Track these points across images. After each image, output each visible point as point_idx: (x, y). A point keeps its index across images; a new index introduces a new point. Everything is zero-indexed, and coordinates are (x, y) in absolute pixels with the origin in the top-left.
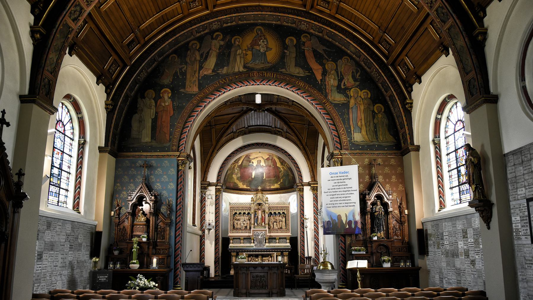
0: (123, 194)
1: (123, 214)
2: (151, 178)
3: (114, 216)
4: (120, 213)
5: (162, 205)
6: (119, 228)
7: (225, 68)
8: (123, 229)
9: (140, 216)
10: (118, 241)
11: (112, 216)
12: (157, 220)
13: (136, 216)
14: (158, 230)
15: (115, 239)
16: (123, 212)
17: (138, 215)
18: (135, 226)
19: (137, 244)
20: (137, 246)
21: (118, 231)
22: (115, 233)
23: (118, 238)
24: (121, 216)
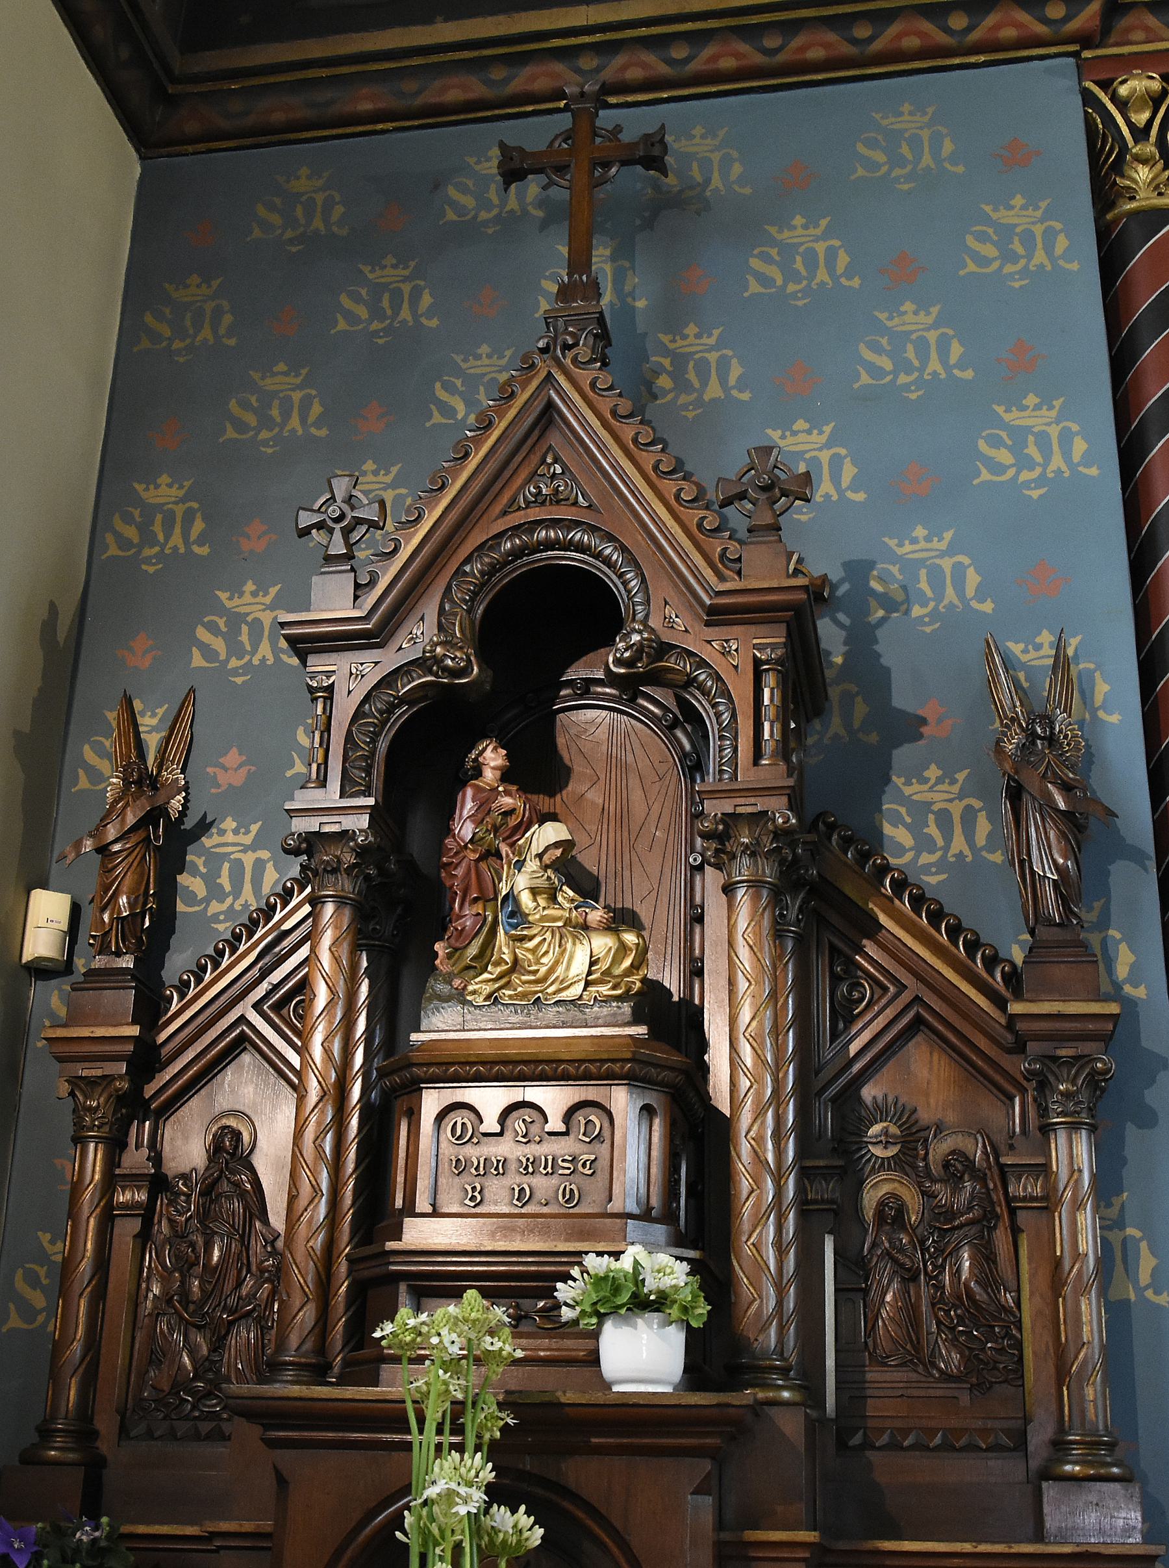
0: (237, 621)
1: (224, 929)
2: (680, 360)
3: (67, 968)
4: (166, 921)
5: (902, 755)
6: (135, 1159)
7: (888, 829)
8: (209, 1190)
9: (517, 914)
10: (105, 1423)
11: (41, 970)
12: (844, 1015)
13: (439, 924)
14: (871, 1198)
15: (55, 1376)
16: (216, 892)
17: (487, 896)
18: (432, 1102)
19: (495, 1452)
20: (496, 1494)
21: (127, 1229)
22: (68, 1266)
23: (116, 1357)
24: (177, 963)
